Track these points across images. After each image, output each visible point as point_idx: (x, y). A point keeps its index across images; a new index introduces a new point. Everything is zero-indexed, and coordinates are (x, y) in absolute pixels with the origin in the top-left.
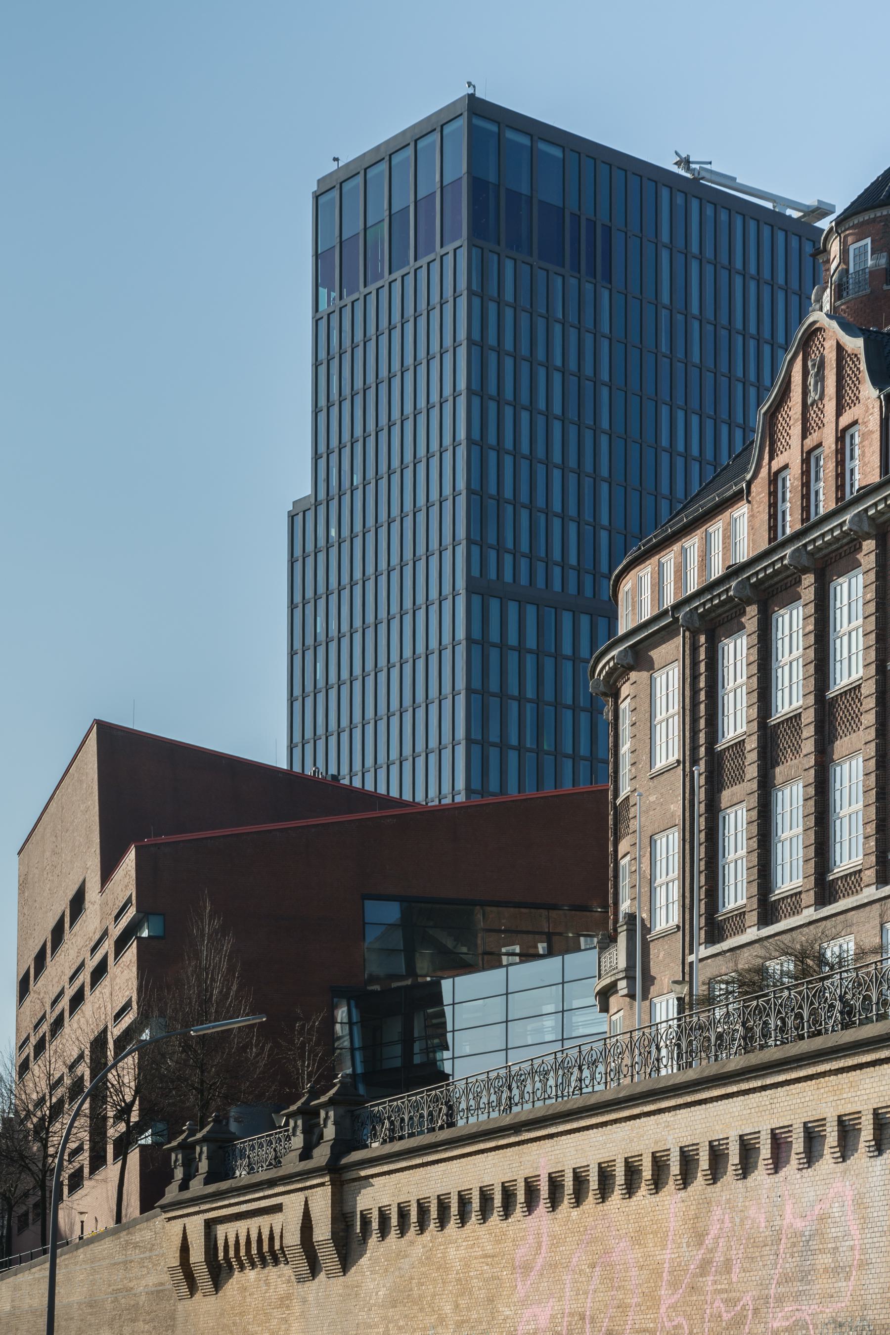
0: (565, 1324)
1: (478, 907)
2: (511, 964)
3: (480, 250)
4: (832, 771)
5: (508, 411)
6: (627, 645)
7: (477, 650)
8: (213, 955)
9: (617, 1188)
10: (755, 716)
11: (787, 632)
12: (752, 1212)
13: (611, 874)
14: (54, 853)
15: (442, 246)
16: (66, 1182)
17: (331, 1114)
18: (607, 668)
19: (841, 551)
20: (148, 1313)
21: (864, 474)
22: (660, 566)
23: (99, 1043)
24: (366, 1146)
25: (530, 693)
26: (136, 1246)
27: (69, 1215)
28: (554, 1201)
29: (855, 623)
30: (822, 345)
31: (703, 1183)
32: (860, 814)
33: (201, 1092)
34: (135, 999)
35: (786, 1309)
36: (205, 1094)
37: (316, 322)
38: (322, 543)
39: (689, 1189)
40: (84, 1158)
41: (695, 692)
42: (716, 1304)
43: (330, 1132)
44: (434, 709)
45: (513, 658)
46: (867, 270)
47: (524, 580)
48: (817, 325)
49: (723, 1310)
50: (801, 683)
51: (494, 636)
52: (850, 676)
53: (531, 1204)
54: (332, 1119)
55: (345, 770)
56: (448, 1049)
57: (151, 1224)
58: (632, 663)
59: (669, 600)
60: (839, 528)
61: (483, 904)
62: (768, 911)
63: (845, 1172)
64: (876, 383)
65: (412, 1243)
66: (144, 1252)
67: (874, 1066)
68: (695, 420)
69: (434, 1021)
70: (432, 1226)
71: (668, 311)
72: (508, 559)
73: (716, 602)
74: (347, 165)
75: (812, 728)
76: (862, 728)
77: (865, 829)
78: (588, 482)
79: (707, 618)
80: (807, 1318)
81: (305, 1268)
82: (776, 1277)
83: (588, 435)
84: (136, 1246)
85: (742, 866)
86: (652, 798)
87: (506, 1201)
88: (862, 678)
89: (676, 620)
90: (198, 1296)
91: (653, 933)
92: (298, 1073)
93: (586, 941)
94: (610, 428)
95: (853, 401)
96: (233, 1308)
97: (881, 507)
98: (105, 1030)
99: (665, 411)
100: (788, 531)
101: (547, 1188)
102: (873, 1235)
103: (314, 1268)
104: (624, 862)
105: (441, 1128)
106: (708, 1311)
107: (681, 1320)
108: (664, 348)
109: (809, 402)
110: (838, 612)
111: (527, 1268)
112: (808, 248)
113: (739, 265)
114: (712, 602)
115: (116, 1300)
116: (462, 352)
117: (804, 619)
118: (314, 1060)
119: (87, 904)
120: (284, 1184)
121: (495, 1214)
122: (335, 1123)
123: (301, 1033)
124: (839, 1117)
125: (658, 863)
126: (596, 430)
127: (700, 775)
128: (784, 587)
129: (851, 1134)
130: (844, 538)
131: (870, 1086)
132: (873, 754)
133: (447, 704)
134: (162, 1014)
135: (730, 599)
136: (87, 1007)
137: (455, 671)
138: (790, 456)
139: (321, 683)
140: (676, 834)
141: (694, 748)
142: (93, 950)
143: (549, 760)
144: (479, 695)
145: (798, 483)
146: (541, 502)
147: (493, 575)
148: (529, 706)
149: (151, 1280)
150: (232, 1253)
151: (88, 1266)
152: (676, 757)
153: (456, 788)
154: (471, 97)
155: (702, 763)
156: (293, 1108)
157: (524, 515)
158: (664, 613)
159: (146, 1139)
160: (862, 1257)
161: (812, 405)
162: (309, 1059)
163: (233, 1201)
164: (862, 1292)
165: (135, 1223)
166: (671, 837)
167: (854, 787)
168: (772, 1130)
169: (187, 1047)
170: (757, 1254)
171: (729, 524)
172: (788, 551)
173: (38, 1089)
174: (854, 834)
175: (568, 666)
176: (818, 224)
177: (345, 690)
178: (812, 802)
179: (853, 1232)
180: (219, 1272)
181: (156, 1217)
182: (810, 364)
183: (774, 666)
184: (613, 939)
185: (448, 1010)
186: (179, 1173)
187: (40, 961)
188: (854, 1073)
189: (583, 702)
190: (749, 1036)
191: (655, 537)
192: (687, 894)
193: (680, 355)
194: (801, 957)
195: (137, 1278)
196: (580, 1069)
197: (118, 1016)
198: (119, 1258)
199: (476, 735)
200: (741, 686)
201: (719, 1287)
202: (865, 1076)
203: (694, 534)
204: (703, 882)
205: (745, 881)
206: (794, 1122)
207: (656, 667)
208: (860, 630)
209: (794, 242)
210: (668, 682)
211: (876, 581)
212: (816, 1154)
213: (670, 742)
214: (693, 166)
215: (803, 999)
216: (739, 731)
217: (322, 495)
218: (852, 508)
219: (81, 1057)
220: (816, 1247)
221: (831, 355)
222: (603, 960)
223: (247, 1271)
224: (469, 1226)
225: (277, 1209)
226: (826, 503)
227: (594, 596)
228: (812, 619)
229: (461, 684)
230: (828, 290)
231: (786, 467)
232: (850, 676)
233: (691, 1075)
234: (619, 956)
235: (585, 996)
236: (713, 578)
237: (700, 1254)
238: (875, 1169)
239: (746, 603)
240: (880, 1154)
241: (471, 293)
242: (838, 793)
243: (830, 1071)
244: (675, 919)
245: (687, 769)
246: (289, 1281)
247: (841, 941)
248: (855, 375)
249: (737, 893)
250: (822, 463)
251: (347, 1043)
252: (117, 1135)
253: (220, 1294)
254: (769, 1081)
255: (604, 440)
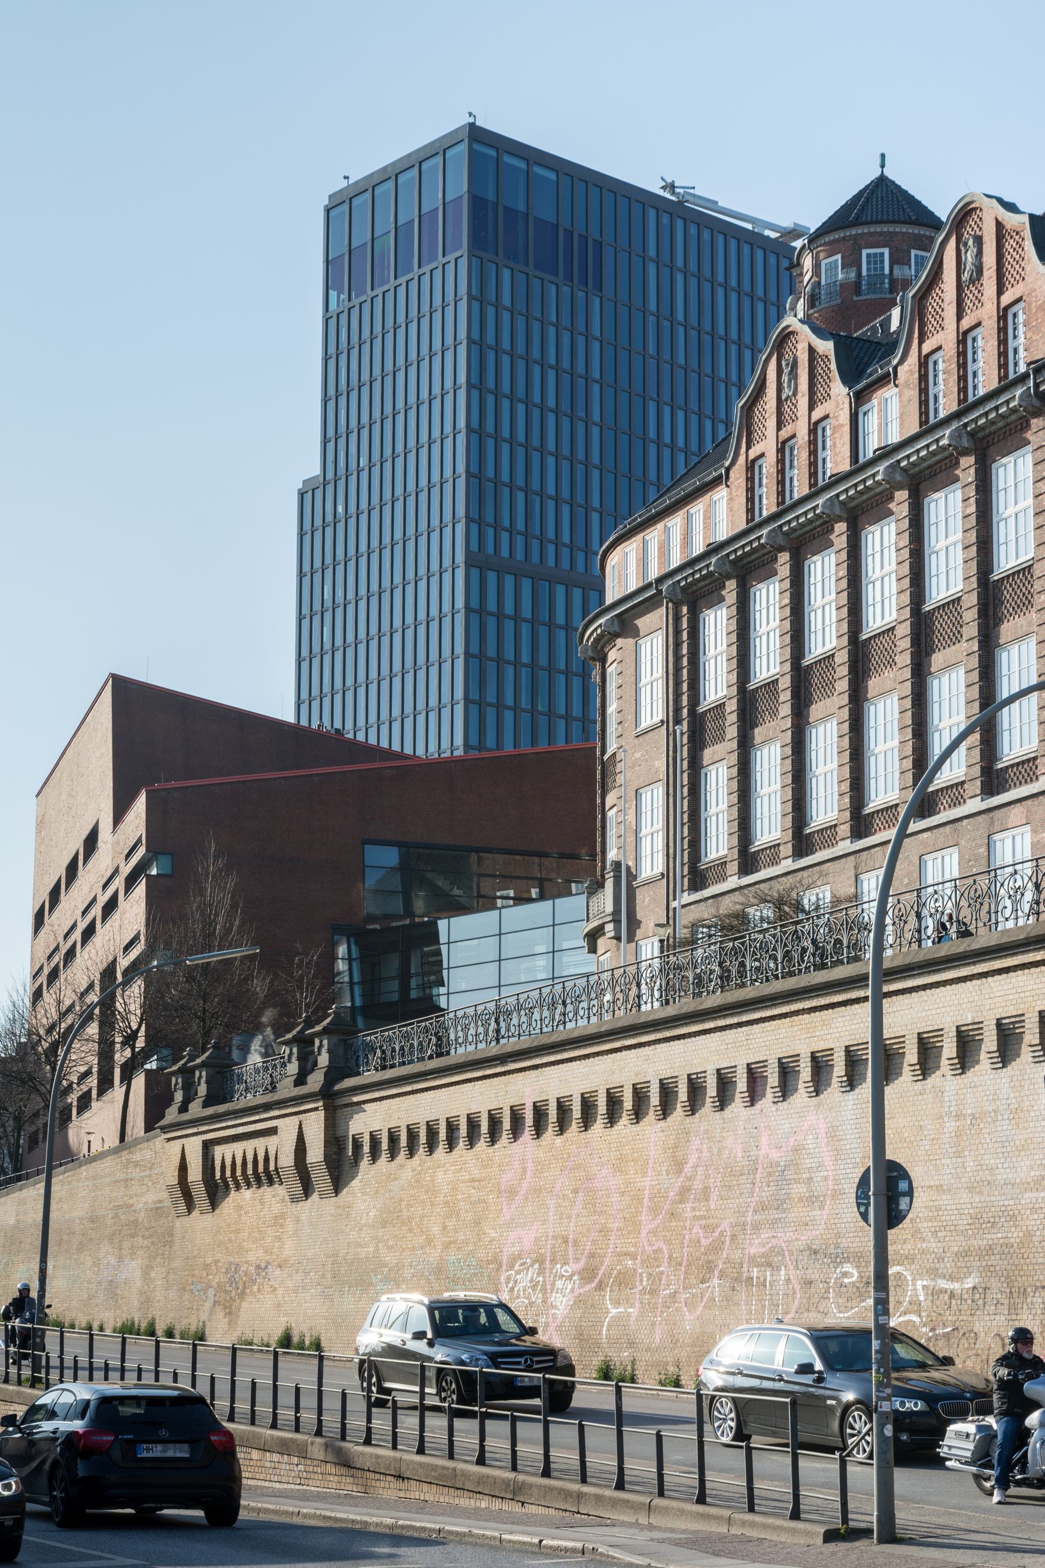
0: (549, 1246)
1: (473, 854)
2: (503, 907)
3: (479, 261)
4: (808, 733)
5: (506, 404)
7: (475, 618)
8: (217, 892)
9: (599, 1117)
10: (735, 681)
11: (764, 604)
12: (729, 1142)
13: (599, 824)
14: (70, 795)
15: (444, 256)
16: (75, 1103)
17: (325, 1042)
20: (147, 1229)
21: (836, 463)
22: (645, 542)
23: (109, 973)
24: (358, 1074)
25: (525, 659)
26: (136, 1165)
27: (78, 1135)
28: (539, 1129)
31: (682, 1113)
32: (835, 773)
33: (203, 1020)
34: (143, 930)
35: (763, 1236)
36: (208, 1022)
37: (327, 321)
38: (329, 518)
39: (668, 1119)
40: (93, 1082)
41: (678, 658)
42: (695, 1230)
43: (324, 1060)
44: (434, 671)
45: (509, 626)
47: (520, 555)
48: (790, 329)
49: (702, 1235)
50: (778, 651)
51: (492, 605)
52: (824, 646)
53: (516, 1130)
54: (326, 1047)
55: (349, 725)
56: (443, 985)
57: (151, 1144)
58: (618, 630)
59: (654, 574)
61: (478, 850)
62: (748, 861)
63: (818, 1106)
65: (402, 1166)
66: (144, 1171)
67: (845, 1006)
68: (680, 414)
69: (431, 959)
70: (422, 1151)
72: (505, 536)
73: (697, 576)
74: (357, 182)
75: (788, 693)
76: (836, 694)
77: (839, 786)
78: (580, 469)
79: (690, 591)
80: (783, 1244)
81: (298, 1189)
82: (753, 1205)
83: (580, 427)
84: (136, 1165)
85: (724, 819)
86: (638, 755)
87: (493, 1128)
89: (660, 592)
90: (196, 1213)
91: (639, 880)
92: (296, 1004)
93: (577, 888)
96: (229, 1225)
97: (851, 492)
98: (114, 961)
99: (652, 406)
100: (765, 513)
101: (532, 1116)
102: (846, 1166)
103: (307, 1188)
104: (610, 814)
105: (431, 1057)
106: (687, 1237)
107: (661, 1244)
108: (651, 349)
109: (783, 397)
110: (812, 587)
111: (512, 1192)
112: (785, 263)
113: (721, 278)
115: (116, 1216)
116: (462, 350)
118: (312, 992)
119: (100, 844)
120: (279, 1108)
121: (482, 1140)
122: (329, 1051)
123: (300, 967)
124: (812, 1053)
125: (643, 815)
126: (587, 421)
127: (682, 734)
129: (824, 1070)
131: (842, 1024)
132: (847, 718)
133: (447, 667)
134: (168, 946)
135: (710, 574)
136: (99, 939)
137: (455, 637)
138: (766, 445)
139: (327, 646)
140: (661, 789)
141: (678, 710)
142: (105, 886)
143: (543, 720)
144: (479, 662)
146: (536, 486)
147: (490, 550)
148: (524, 671)
149: (151, 1198)
150: (228, 1173)
151: (90, 1183)
152: (660, 717)
153: (455, 744)
154: (472, 126)
155: (685, 723)
156: (289, 1036)
157: (520, 497)
158: (649, 586)
159: (152, 1065)
160: (836, 1187)
161: (786, 400)
162: (307, 991)
163: (230, 1123)
164: (836, 1221)
165: (137, 1142)
166: (655, 791)
167: (829, 748)
168: (748, 1065)
169: (190, 978)
170: (734, 1183)
172: (765, 531)
173: (49, 1016)
174: (829, 791)
175: (561, 635)
176: (793, 244)
177: (350, 652)
178: (789, 761)
179: (826, 1164)
180: (216, 1191)
181: (157, 1137)
182: (784, 363)
183: (752, 636)
184: (601, 885)
185: (444, 949)
186: (179, 1096)
187: (55, 895)
188: (826, 1012)
189: (575, 667)
190: (725, 977)
191: (640, 516)
192: (671, 844)
193: (667, 356)
194: (779, 903)
195: (137, 1195)
196: (564, 1003)
197: (127, 948)
198: (120, 1176)
199: (474, 696)
200: (721, 653)
201: (698, 1214)
202: (837, 1015)
204: (686, 833)
205: (726, 834)
206: (769, 1057)
207: (642, 634)
208: (833, 604)
209: (772, 259)
210: (651, 649)
212: (791, 1088)
213: (655, 704)
214: (677, 190)
215: (777, 942)
216: (720, 694)
217: (330, 475)
219: (91, 986)
220: (791, 1177)
222: (591, 904)
223: (242, 1191)
224: (456, 1152)
225: (273, 1131)
226: (800, 488)
228: (788, 593)
229: (460, 649)
231: (762, 455)
232: (824, 646)
233: (671, 1011)
234: (606, 900)
235: (574, 938)
237: (679, 1181)
238: (848, 1103)
240: (852, 1089)
241: (471, 297)
242: (814, 754)
243: (804, 1009)
244: (660, 867)
245: (671, 729)
246: (283, 1201)
247: (817, 890)
249: (719, 842)
250: (796, 452)
251: (347, 979)
252: (123, 1060)
253: (217, 1212)
254: (745, 1018)
255: (595, 431)
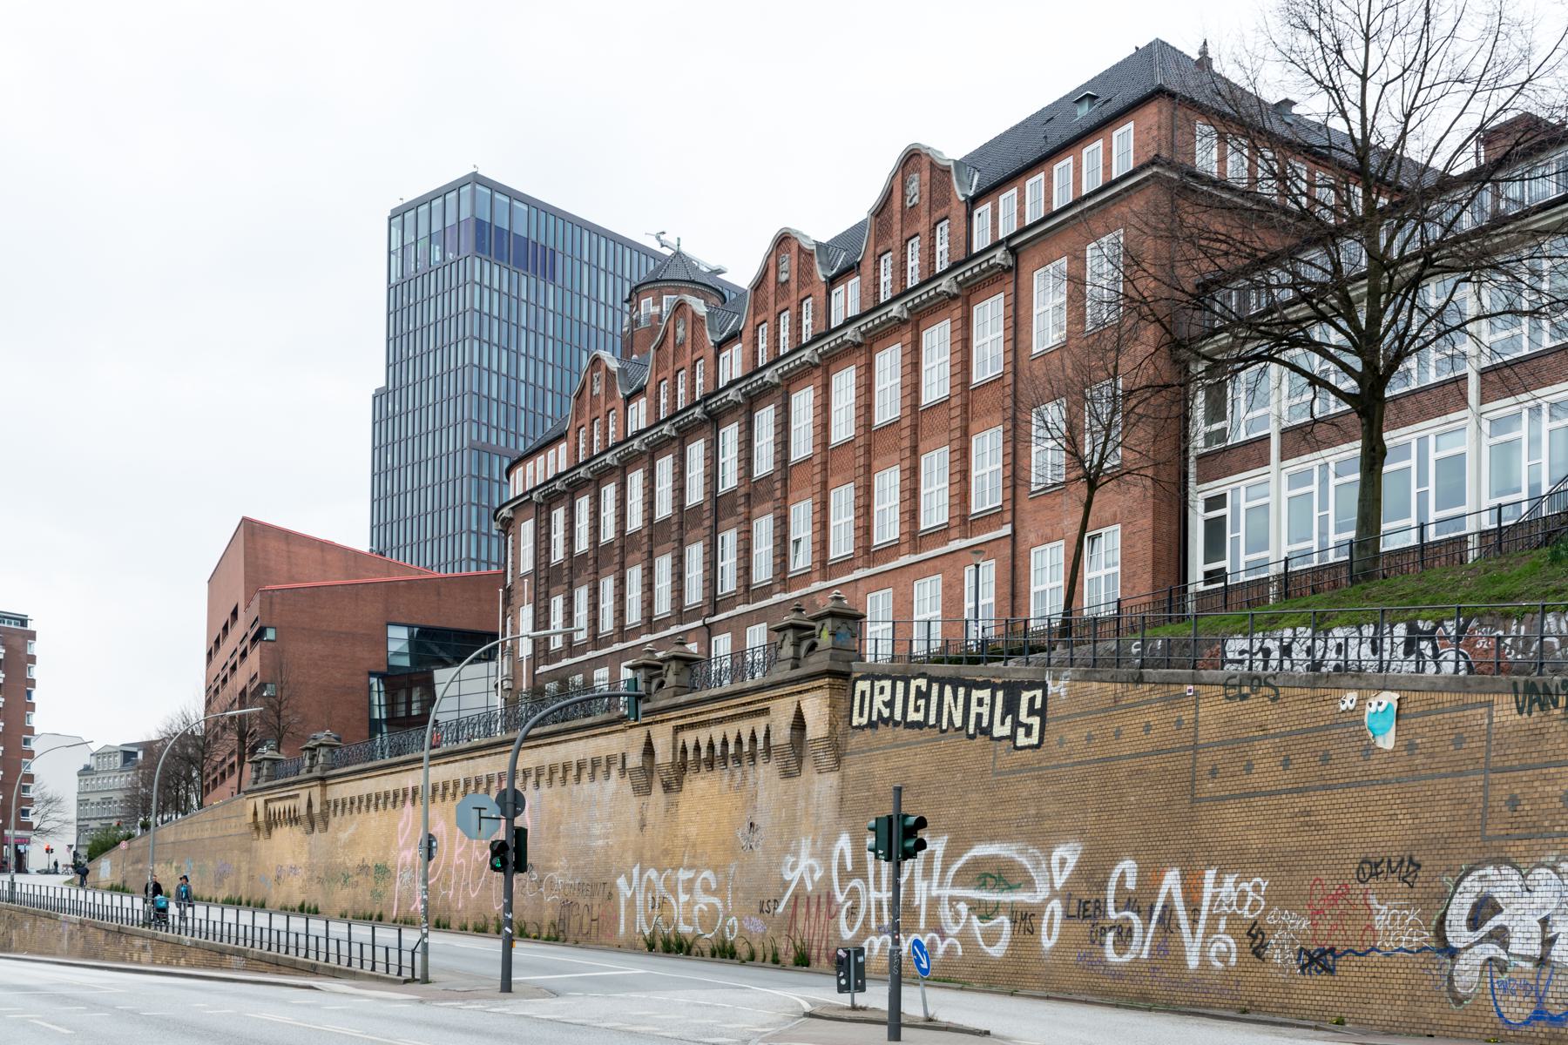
47: (503, 444)
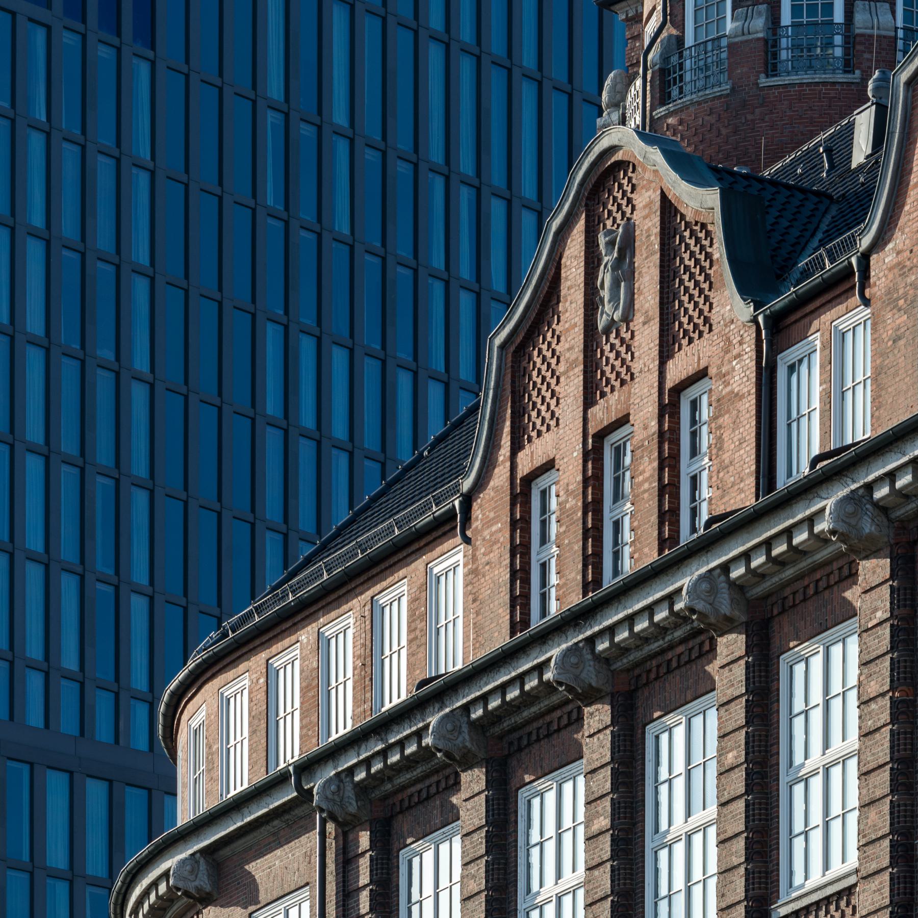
6: (196, 848)
11: (428, 889)
18: (153, 897)
19: (670, 655)
21: (721, 488)
29: (699, 817)
30: (629, 201)
46: (724, 42)
48: (619, 156)
58: (208, 888)
59: (291, 750)
60: (666, 604)
64: (745, 288)
71: (280, 117)
73: (394, 758)
79: (377, 794)
88: (857, 871)
89: (306, 795)
94: (153, 370)
95: (696, 326)
97: (758, 561)
99: (272, 336)
100: (554, 608)
108: (271, 196)
109: (601, 324)
114: (385, 759)
117: (588, 803)
126: (119, 373)
128: (543, 732)
130: (676, 626)
135: (425, 754)
138: (560, 443)
145: (575, 503)
158: (279, 781)
161: (607, 331)
171: (424, 587)
172: (555, 652)
182: (602, 240)
183: (649, 845)
193: (307, 213)
203: (345, 607)
207: (263, 897)
208: (712, 832)
211: (748, 723)
218: (694, 564)
221: (648, 224)
226: (636, 549)
227: (117, 741)
228: (607, 803)
230: (639, 82)
231: (549, 466)
236: (387, 706)
239: (460, 764)
248: (702, 269)
250: (628, 460)
255: (139, 394)
